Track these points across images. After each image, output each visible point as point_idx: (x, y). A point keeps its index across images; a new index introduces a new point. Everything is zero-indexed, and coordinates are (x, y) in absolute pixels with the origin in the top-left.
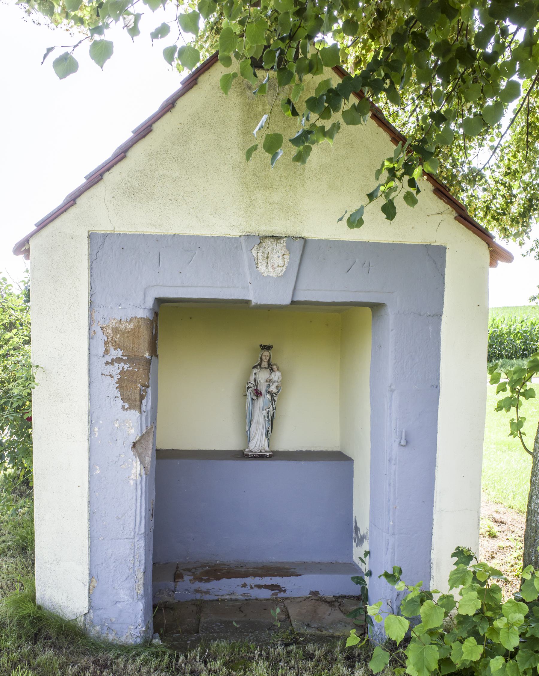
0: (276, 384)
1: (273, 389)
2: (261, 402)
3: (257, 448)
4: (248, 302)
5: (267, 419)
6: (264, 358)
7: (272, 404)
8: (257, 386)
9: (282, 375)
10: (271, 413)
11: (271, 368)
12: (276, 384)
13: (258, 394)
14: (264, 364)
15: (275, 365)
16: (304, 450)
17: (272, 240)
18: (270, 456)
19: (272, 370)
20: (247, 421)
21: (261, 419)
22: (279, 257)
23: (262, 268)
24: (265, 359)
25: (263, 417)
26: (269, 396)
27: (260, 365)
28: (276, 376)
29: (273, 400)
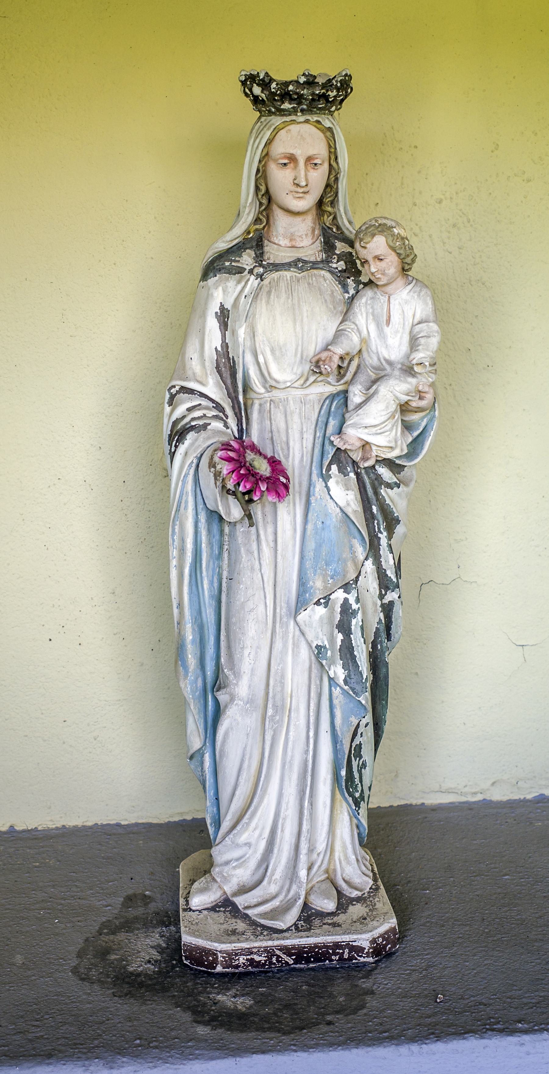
0: (395, 390)
1: (374, 427)
2: (280, 539)
5: (339, 672)
6: (281, 179)
8: (242, 413)
9: (441, 314)
10: (369, 616)
11: (344, 261)
12: (395, 390)
13: (253, 477)
15: (383, 229)
18: (377, 950)
19: (352, 273)
20: (189, 686)
21: (296, 671)
24: (296, 189)
25: (305, 653)
26: (342, 494)
28: (393, 321)
29: (378, 519)
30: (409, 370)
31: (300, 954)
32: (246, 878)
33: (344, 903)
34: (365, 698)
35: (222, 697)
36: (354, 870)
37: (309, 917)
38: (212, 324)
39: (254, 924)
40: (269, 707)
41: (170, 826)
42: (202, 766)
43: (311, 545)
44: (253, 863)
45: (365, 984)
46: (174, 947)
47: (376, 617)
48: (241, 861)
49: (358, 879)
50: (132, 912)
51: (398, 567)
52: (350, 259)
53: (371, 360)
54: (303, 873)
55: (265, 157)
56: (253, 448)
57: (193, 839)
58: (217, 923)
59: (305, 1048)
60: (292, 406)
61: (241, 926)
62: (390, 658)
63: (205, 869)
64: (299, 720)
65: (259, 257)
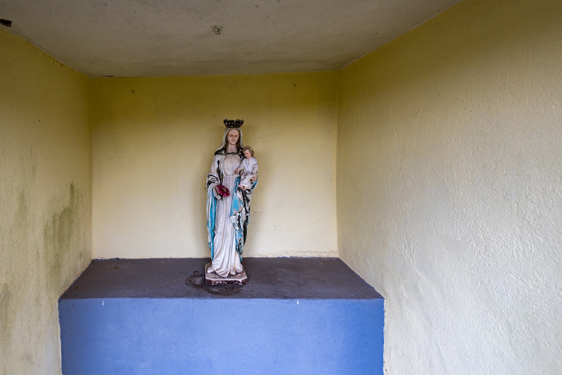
0: (249, 177)
1: (246, 184)
2: (226, 204)
5: (237, 228)
6: (230, 139)
8: (221, 179)
10: (243, 218)
11: (241, 152)
12: (249, 177)
13: (223, 192)
15: (248, 149)
18: (243, 283)
19: (243, 156)
20: (209, 230)
21: (229, 227)
25: (231, 225)
26: (239, 195)
28: (249, 164)
29: (246, 200)
30: (252, 173)
31: (228, 282)
33: (237, 273)
34: (242, 233)
35: (215, 232)
37: (230, 275)
38: (216, 163)
39: (219, 276)
40: (224, 234)
41: (202, 259)
42: (210, 247)
43: (233, 204)
44: (220, 264)
45: (240, 288)
46: (204, 280)
47: (245, 218)
48: (217, 264)
49: (240, 269)
50: (195, 274)
51: (249, 209)
52: (242, 152)
53: (245, 171)
54: (229, 267)
55: (227, 135)
56: (223, 187)
57: (208, 261)
58: (213, 275)
59: (229, 298)
60: (231, 179)
61: (217, 276)
62: (247, 226)
63: (211, 265)
64: (230, 237)
65: (225, 152)
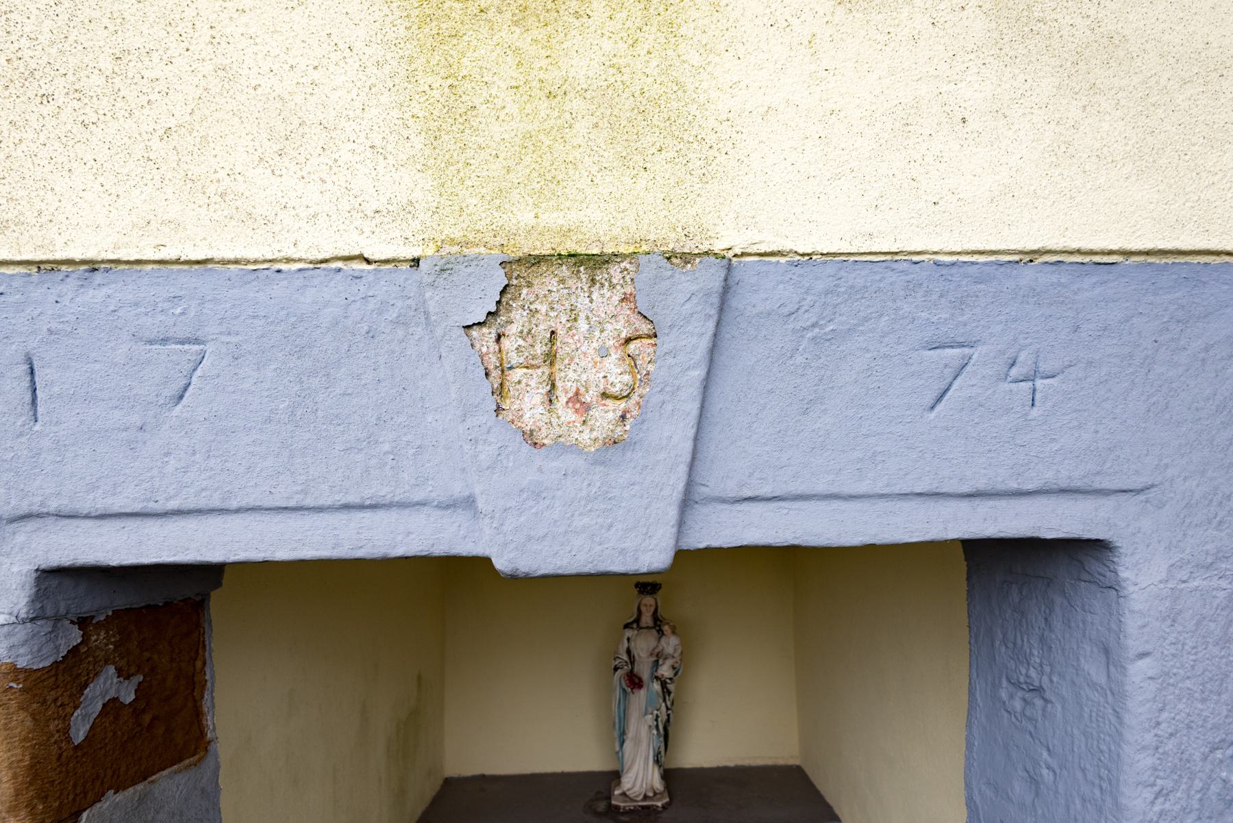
1: (665, 671)
2: (639, 699)
3: (637, 789)
4: (486, 561)
5: (655, 732)
6: (643, 609)
7: (664, 700)
8: (632, 663)
11: (658, 624)
12: (669, 662)
14: (647, 619)
16: (732, 764)
17: (565, 271)
18: (663, 807)
19: (661, 633)
21: (644, 731)
22: (604, 353)
23: (529, 404)
26: (657, 686)
27: (637, 621)
28: (671, 644)
29: (666, 691)
31: (643, 807)
32: (24, 610)
33: (655, 794)
36: (658, 784)
37: (646, 797)
42: (619, 756)
46: (610, 805)
47: (665, 717)
58: (622, 798)
63: (619, 784)
